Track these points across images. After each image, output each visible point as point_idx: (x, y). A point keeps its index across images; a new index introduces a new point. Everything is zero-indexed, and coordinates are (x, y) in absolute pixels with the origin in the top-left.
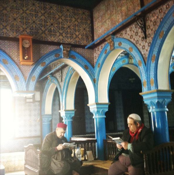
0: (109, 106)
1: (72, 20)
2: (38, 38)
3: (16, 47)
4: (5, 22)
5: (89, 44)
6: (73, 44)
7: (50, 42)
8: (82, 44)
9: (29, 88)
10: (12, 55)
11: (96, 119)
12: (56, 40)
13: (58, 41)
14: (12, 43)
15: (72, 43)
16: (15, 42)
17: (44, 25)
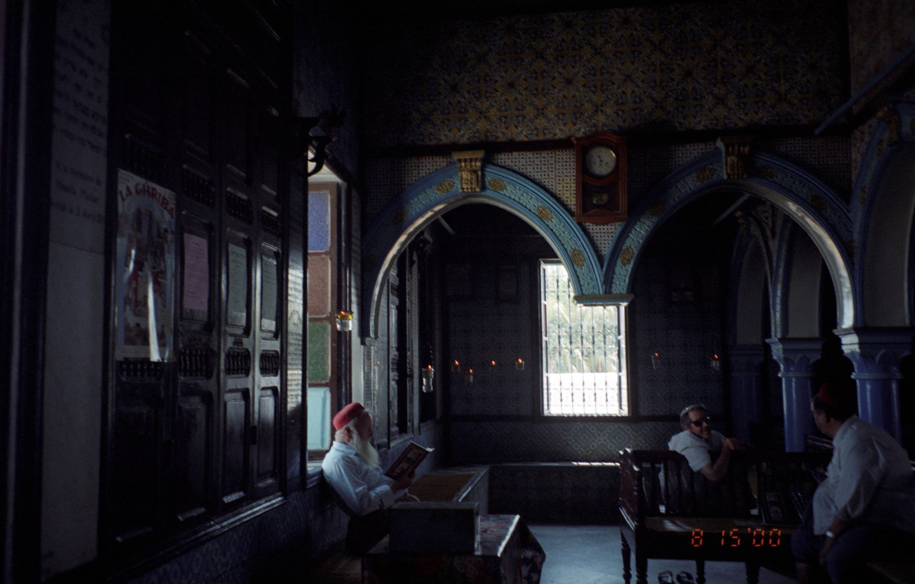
5: (831, 115)
9: (614, 285)
10: (561, 193)
11: (863, 381)
17: (661, 82)
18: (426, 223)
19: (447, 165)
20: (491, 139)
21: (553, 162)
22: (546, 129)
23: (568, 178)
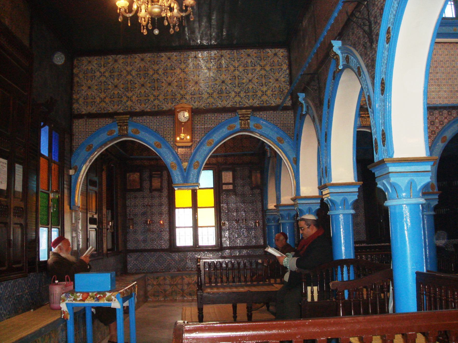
0: (439, 196)
1: (255, 70)
2: (203, 105)
3: (171, 123)
4: (156, 91)
6: (258, 106)
7: (220, 108)
8: (272, 105)
12: (230, 104)
13: (233, 106)
14: (166, 119)
15: (256, 105)
16: (171, 117)
18: (318, 131)
19: (112, 123)
20: (133, 110)
21: (162, 121)
22: (132, 107)
23: (169, 129)
